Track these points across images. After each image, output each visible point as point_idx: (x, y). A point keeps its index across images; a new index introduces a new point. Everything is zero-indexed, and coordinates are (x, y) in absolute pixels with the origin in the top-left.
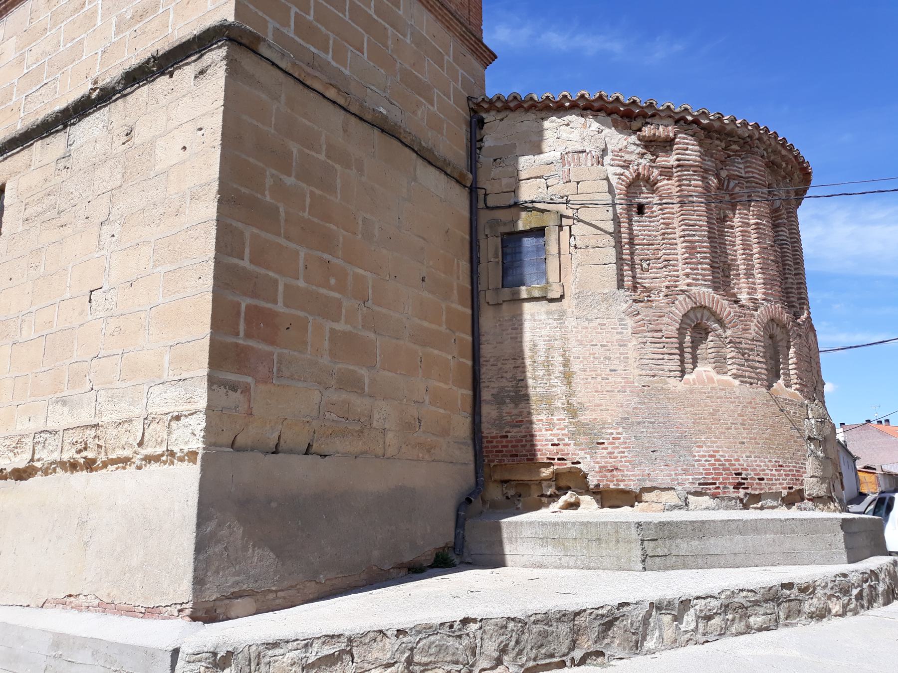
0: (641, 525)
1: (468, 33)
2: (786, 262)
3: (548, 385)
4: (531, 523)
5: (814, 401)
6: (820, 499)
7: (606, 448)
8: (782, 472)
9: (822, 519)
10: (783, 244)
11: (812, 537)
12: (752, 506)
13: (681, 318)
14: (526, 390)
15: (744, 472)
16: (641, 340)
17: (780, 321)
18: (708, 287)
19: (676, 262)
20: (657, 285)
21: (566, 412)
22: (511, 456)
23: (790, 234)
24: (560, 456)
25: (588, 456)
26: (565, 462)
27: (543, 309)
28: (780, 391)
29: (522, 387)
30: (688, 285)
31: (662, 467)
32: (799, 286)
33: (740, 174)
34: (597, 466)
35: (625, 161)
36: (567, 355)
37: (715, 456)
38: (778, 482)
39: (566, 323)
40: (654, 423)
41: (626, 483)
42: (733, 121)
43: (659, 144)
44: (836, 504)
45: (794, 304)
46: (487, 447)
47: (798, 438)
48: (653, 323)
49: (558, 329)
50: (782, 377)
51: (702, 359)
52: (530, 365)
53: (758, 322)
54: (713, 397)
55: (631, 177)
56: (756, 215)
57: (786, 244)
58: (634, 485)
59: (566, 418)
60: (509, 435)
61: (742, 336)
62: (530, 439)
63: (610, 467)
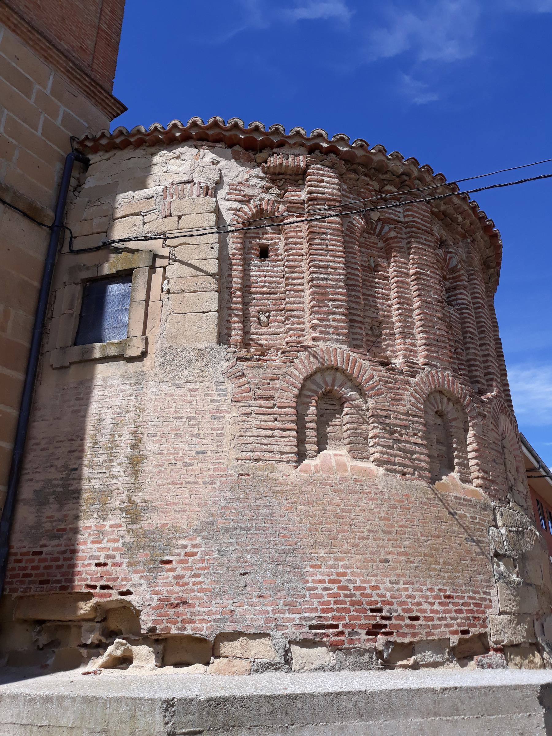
0: (173, 706)
1: (78, 71)
2: (467, 329)
3: (107, 475)
4: (14, 697)
5: (509, 503)
6: (516, 649)
7: (173, 570)
8: (450, 606)
9: (506, 687)
10: (463, 309)
11: (488, 721)
12: (399, 663)
13: (302, 382)
14: (79, 483)
15: (386, 608)
16: (243, 410)
17: (452, 393)
18: (342, 342)
19: (301, 313)
20: (278, 342)
21: (124, 515)
22: (41, 582)
23: (473, 298)
24: (104, 583)
25: (144, 583)
26: (111, 591)
27: (119, 372)
28: (451, 487)
29: (74, 479)
30: (314, 339)
31: (254, 600)
32: (485, 359)
33: (397, 218)
34: (155, 598)
35: (244, 196)
36: (139, 432)
37: (340, 581)
38: (443, 623)
39: (145, 389)
40: (249, 529)
41: (196, 625)
42: (383, 151)
43: (288, 177)
44: (545, 655)
45: (479, 379)
46: (13, 569)
47: (477, 554)
48: (262, 387)
49: (134, 397)
50: (457, 468)
51: (335, 439)
52: (89, 447)
53: (416, 391)
54: (342, 491)
55: (250, 213)
56: (416, 263)
57: (467, 309)
58: (208, 629)
59: (124, 524)
60: (44, 550)
61: (391, 408)
62: (70, 555)
63: (176, 599)
